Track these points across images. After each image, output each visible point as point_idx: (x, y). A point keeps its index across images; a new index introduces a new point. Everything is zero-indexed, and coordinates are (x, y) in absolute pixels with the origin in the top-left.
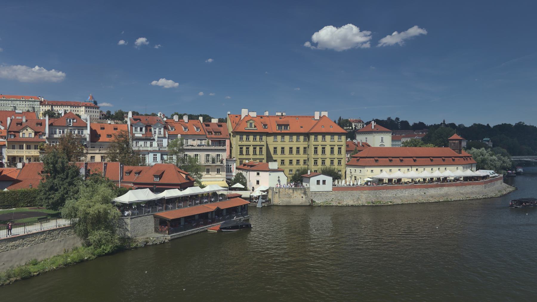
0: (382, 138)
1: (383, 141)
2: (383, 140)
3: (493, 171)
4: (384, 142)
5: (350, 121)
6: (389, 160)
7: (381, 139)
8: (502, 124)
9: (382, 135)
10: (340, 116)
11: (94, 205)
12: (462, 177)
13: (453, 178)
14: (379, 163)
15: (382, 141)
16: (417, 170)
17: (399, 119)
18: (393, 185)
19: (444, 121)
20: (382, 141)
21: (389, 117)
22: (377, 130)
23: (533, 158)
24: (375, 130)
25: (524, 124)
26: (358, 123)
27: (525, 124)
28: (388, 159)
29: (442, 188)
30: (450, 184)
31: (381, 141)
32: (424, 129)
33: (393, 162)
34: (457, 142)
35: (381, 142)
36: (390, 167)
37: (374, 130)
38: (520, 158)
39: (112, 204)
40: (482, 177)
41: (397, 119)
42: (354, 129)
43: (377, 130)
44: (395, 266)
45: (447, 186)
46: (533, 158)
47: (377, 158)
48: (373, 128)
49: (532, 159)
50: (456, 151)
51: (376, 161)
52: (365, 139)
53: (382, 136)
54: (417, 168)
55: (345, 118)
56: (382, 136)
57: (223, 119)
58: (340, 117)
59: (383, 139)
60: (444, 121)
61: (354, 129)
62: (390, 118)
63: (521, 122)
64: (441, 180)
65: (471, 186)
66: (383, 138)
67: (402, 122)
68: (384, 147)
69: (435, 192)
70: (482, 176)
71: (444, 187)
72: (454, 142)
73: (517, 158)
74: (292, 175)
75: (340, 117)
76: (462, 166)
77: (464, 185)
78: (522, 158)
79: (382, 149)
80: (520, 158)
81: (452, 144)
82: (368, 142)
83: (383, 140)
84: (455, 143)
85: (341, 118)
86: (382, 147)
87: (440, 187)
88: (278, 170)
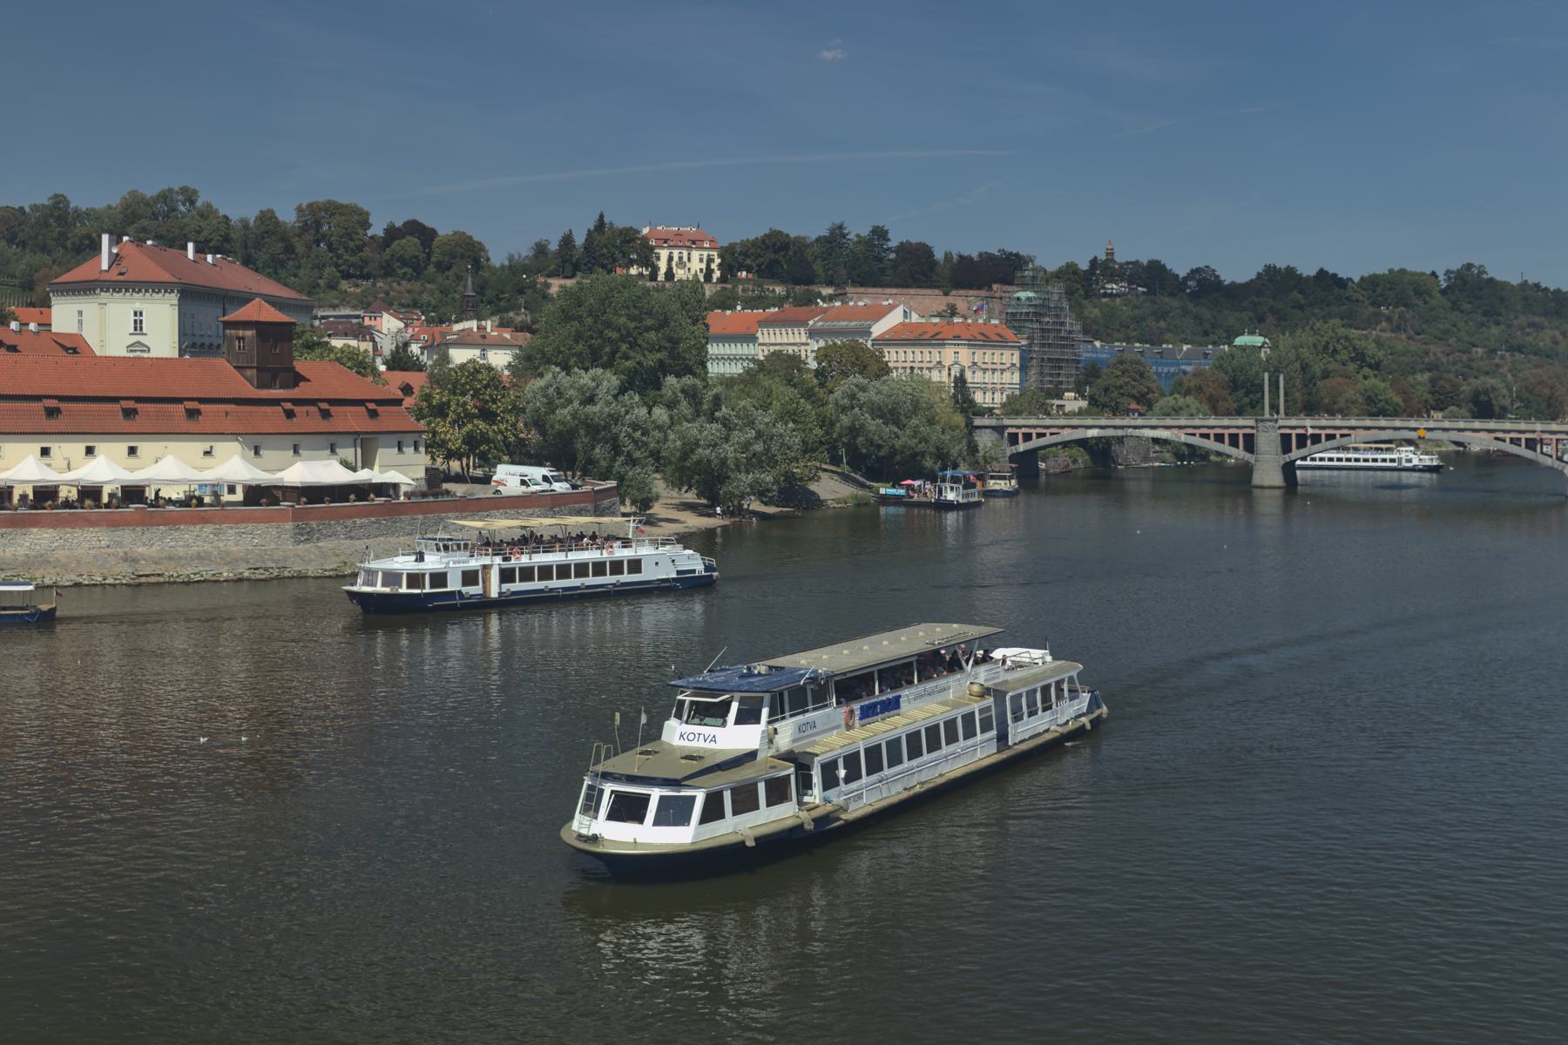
0: (135, 314)
2: (141, 321)
4: (144, 331)
5: (645, 239)
6: (366, 414)
7: (133, 318)
8: (1391, 271)
9: (138, 302)
10: (599, 213)
11: (242, 559)
12: (239, 490)
14: (202, 423)
15: (138, 326)
17: (887, 232)
18: (159, 507)
19: (1110, 253)
20: (138, 326)
21: (838, 222)
23: (1180, 427)
24: (114, 276)
25: (1485, 276)
26: (689, 248)
28: (116, 407)
29: (24, 531)
30: (70, 513)
31: (136, 329)
32: (995, 287)
33: (200, 418)
34: (249, 333)
35: (132, 330)
41: (880, 233)
43: (121, 278)
44: (1475, 799)
45: (54, 526)
46: (1180, 427)
48: (105, 266)
49: (1176, 431)
53: (138, 306)
56: (138, 306)
58: (602, 216)
60: (1110, 253)
61: (661, 277)
62: (841, 227)
63: (1469, 266)
64: (105, 499)
65: (208, 529)
66: (141, 314)
67: (904, 248)
71: (35, 530)
72: (241, 333)
73: (1115, 427)
75: (602, 216)
78: (1135, 427)
79: (136, 364)
81: (234, 345)
83: (144, 325)
86: (138, 354)
88: (333, 439)
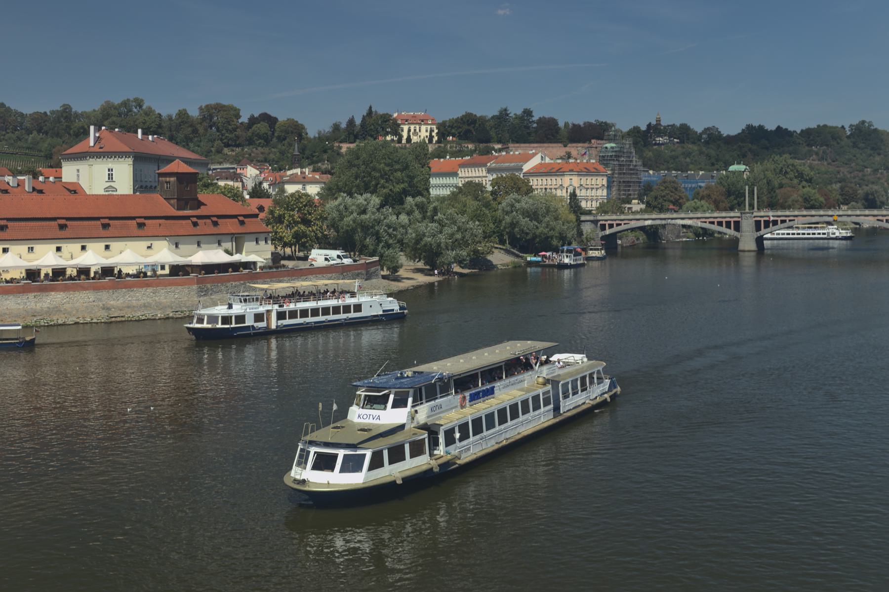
0: (109, 170)
1: (112, 178)
2: (112, 174)
3: (338, 252)
4: (114, 180)
8: (819, 126)
9: (110, 163)
13: (132, 270)
15: (110, 177)
16: (107, 247)
19: (658, 120)
20: (110, 177)
21: (504, 107)
22: (101, 150)
24: (97, 149)
25: (872, 128)
26: (420, 124)
27: (874, 128)
28: (98, 223)
30: (72, 283)
31: (109, 179)
32: (593, 141)
34: (172, 179)
35: (107, 180)
36: (71, 240)
37: (92, 150)
38: (669, 219)
39: (197, 338)
40: (199, 266)
41: (528, 113)
42: (404, 141)
45: (64, 291)
46: (698, 218)
47: (143, 219)
48: (92, 144)
49: (695, 220)
50: (172, 201)
51: (215, 224)
52: (76, 173)
53: (110, 166)
54: (58, 245)
55: (381, 111)
57: (45, 113)
58: (371, 108)
59: (113, 172)
61: (404, 141)
62: (506, 110)
63: (863, 122)
65: (150, 290)
66: (112, 170)
68: (115, 193)
69: (18, 304)
70: (201, 264)
71: (53, 293)
72: (168, 179)
74: (516, 260)
75: (371, 108)
76: (166, 240)
77: (125, 288)
78: (672, 219)
79: (109, 199)
80: (669, 219)
82: (80, 182)
84: (169, 182)
85: (373, 110)
87: (37, 292)
